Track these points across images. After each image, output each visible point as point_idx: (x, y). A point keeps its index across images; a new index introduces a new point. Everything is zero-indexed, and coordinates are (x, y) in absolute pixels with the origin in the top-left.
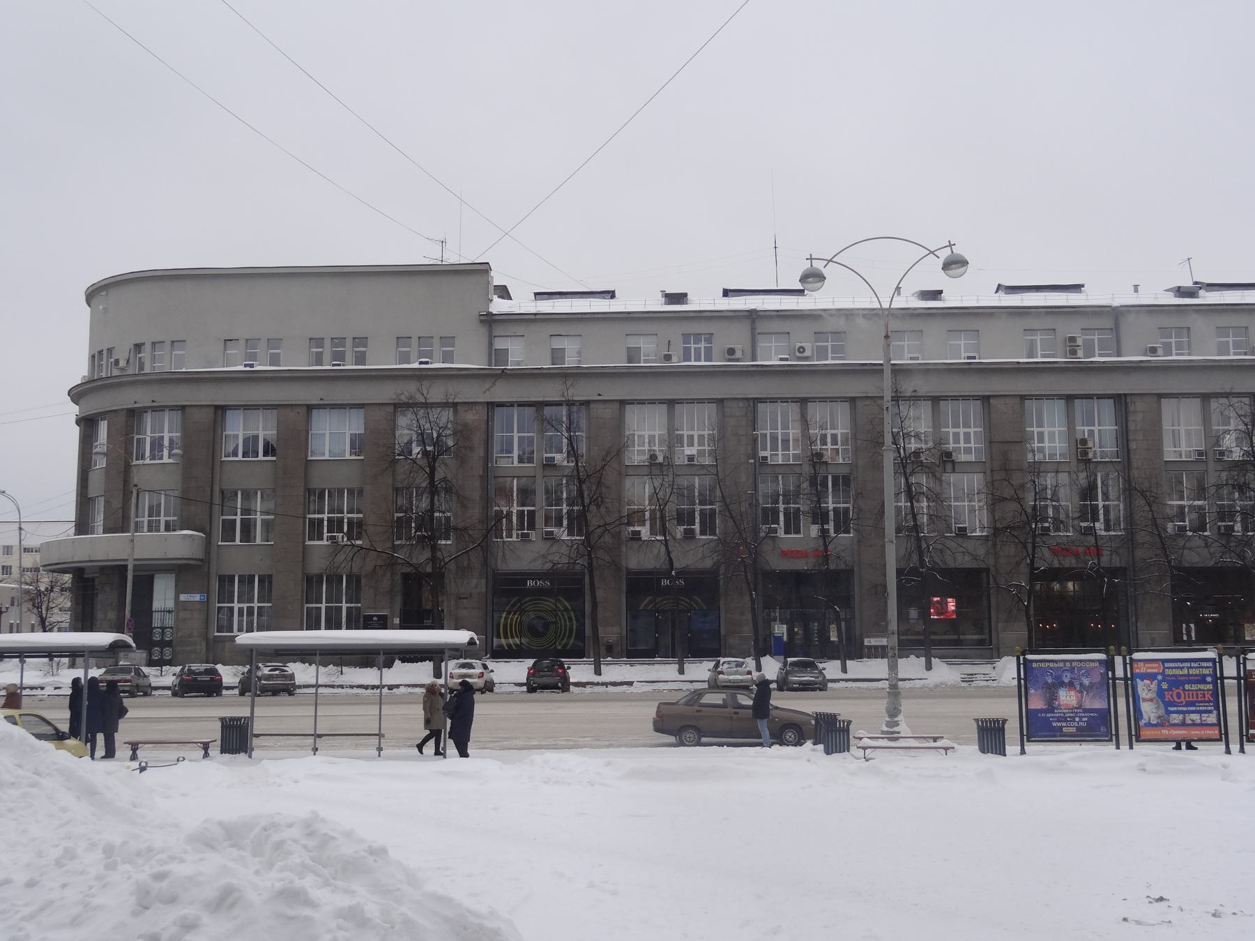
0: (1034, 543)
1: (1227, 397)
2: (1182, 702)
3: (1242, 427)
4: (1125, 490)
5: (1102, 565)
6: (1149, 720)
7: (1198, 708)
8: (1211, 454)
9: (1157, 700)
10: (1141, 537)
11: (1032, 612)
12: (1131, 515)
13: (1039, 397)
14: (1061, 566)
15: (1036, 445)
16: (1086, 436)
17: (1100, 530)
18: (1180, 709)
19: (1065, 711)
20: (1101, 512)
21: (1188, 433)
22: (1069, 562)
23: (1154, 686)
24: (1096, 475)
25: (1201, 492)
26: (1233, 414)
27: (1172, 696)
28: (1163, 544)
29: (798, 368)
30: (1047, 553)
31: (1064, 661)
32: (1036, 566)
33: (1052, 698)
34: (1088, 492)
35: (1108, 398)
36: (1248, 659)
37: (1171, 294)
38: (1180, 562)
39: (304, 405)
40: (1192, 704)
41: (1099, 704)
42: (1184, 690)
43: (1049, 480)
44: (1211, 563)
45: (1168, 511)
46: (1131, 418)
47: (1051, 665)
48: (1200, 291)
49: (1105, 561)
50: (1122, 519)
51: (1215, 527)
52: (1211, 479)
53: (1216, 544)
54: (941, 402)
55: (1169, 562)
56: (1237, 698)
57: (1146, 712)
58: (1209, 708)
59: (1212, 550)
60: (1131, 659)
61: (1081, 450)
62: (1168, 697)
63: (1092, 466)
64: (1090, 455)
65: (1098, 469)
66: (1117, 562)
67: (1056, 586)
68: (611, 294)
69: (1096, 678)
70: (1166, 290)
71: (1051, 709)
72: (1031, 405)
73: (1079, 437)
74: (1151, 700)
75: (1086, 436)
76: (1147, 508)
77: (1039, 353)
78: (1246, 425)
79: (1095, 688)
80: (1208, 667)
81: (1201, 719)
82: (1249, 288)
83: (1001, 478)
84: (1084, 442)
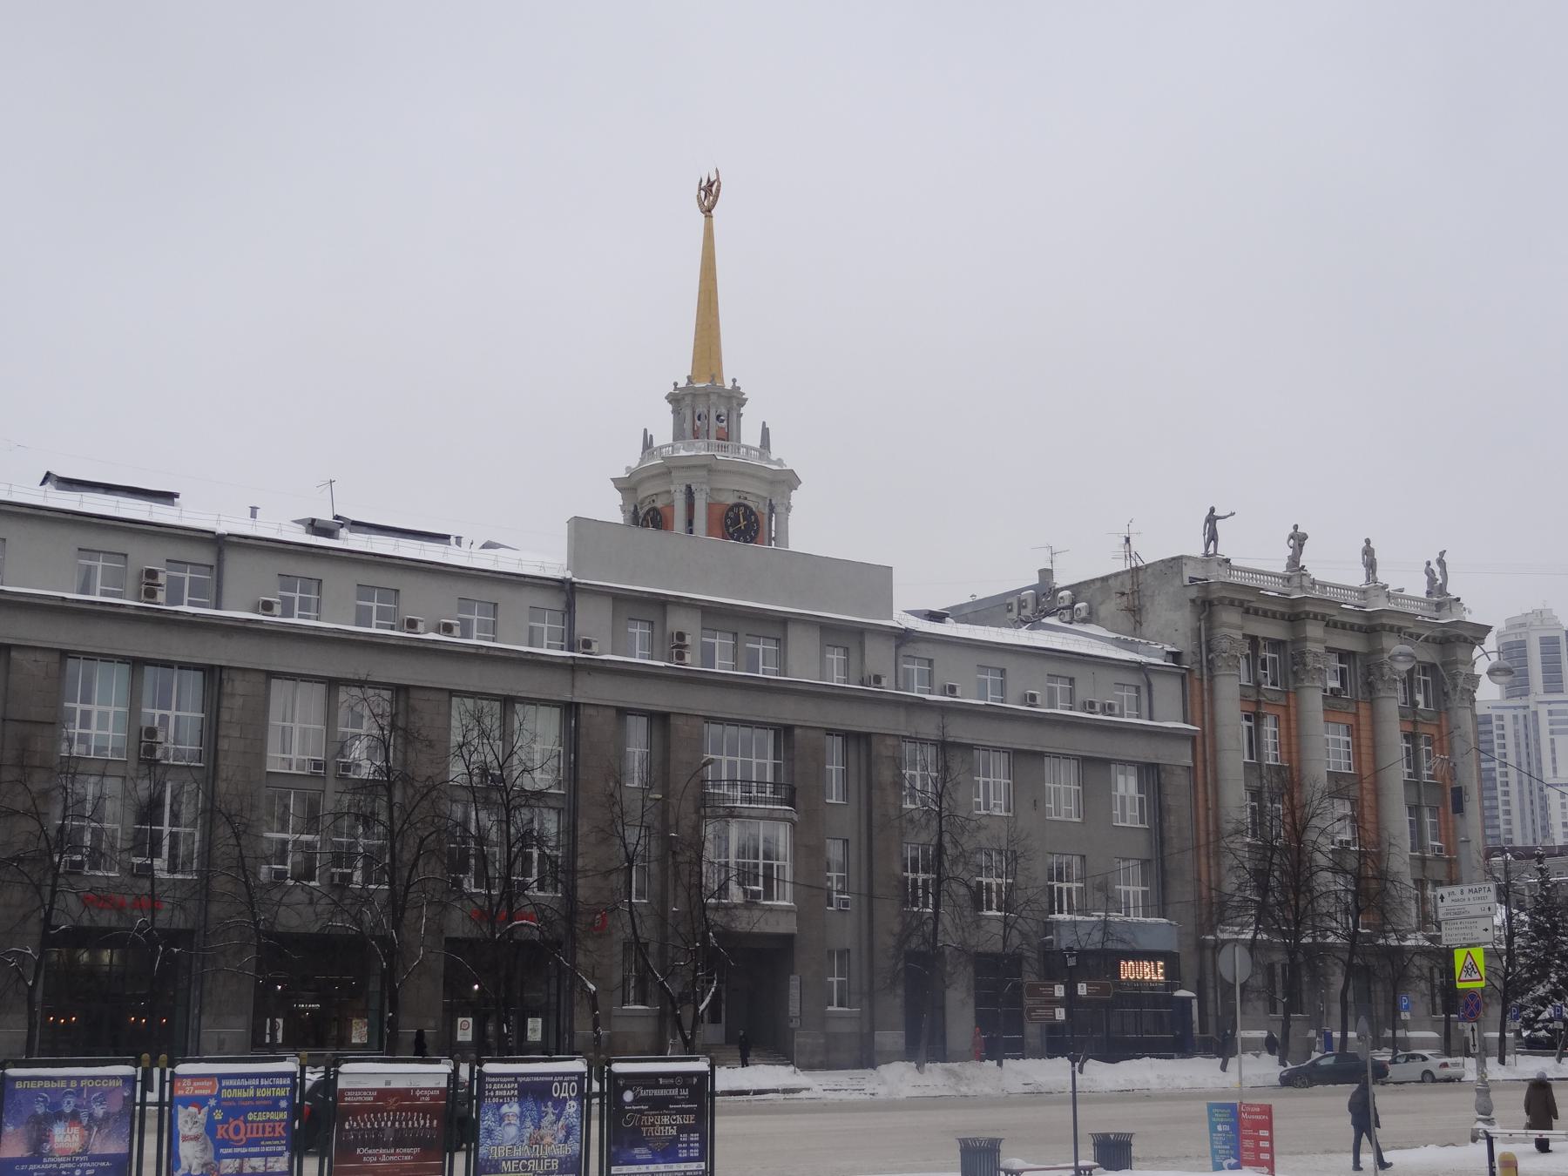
0: (54, 885)
1: (361, 687)
2: (242, 1140)
3: (376, 732)
4: (204, 811)
5: (157, 925)
6: (190, 1170)
7: (263, 1149)
8: (331, 765)
9: (205, 1139)
10: (221, 884)
11: (39, 995)
12: (209, 851)
13: (90, 656)
14: (93, 925)
15: (78, 730)
16: (156, 724)
17: (161, 870)
18: (237, 1150)
19: (60, 1160)
20: (166, 842)
21: (304, 732)
22: (106, 919)
23: (202, 1116)
24: (164, 785)
25: (311, 821)
26: (367, 712)
27: (227, 1131)
28: (251, 897)
29: (443, 647)
30: (72, 900)
31: (68, 1078)
32: (54, 922)
33: (39, 1140)
34: (150, 811)
35: (195, 669)
36: (342, 1073)
37: (302, 528)
38: (272, 924)
39: (57, 649)
40: (254, 1142)
41: (115, 1147)
42: (246, 1121)
43: (91, 789)
44: (315, 929)
45: (265, 845)
46: (225, 703)
47: (47, 1084)
48: (341, 530)
49: (162, 919)
50: (195, 856)
51: (328, 874)
52: (328, 805)
53: (326, 900)
54: (69, 659)
55: (257, 924)
56: (1072, 1106)
57: (186, 1157)
58: (279, 1149)
59: (319, 909)
60: (172, 1074)
61: (145, 743)
62: (221, 1132)
63: (159, 771)
64: (158, 755)
65: (168, 776)
66: (180, 921)
67: (85, 957)
68: (168, 497)
69: (116, 1105)
70: (295, 522)
71: (37, 1155)
72: (76, 668)
73: (145, 724)
74: (196, 1138)
75: (156, 724)
76: (233, 841)
77: (99, 587)
78: (382, 729)
79: (111, 1122)
80: (284, 1086)
81: (265, 1165)
82: (390, 533)
83: (12, 779)
84: (152, 732)
